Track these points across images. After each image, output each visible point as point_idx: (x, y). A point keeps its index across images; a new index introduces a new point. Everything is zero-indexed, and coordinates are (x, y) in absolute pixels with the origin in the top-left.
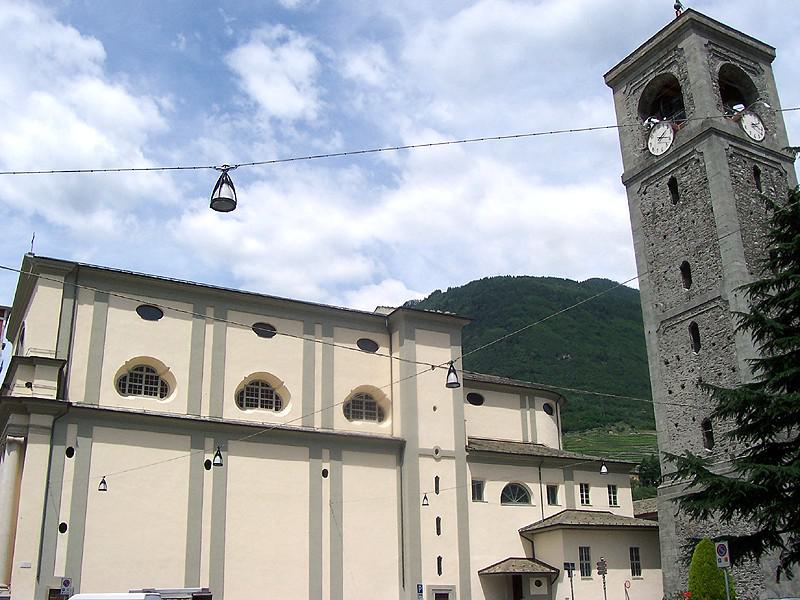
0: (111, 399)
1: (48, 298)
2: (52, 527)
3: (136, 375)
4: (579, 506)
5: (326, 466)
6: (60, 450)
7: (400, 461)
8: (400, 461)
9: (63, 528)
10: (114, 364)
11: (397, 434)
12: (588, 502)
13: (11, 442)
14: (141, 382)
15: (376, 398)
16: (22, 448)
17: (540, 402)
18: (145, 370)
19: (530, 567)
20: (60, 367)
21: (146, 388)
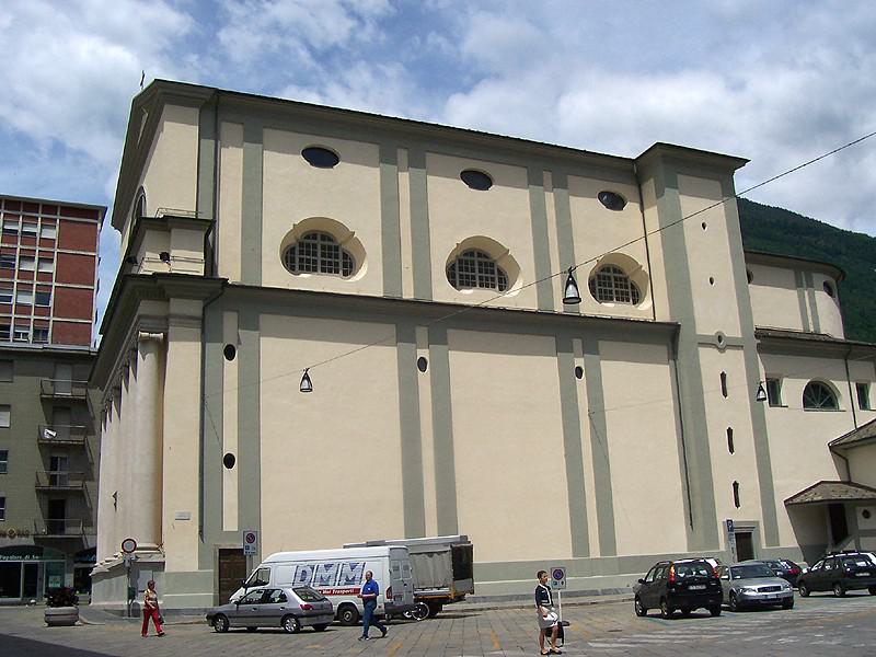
0: (275, 276)
1: (178, 139)
2: (213, 462)
3: (308, 246)
5: (579, 362)
6: (216, 349)
7: (673, 354)
8: (673, 354)
9: (229, 461)
10: (276, 232)
11: (663, 316)
13: (146, 341)
16: (162, 349)
17: (819, 279)
18: (476, 255)
20: (203, 227)
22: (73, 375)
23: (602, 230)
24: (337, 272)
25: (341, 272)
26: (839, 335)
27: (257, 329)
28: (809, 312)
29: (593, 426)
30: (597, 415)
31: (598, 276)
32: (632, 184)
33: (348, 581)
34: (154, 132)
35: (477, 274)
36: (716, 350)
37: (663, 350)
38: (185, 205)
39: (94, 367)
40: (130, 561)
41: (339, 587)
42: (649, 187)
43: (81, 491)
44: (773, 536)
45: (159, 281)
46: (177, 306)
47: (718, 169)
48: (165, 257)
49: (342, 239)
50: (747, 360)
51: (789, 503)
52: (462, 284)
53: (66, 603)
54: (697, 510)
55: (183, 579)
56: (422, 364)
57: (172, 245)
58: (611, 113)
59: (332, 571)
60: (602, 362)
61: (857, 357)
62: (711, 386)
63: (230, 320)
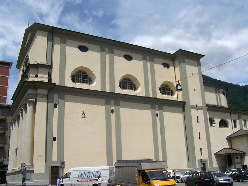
0: (69, 83)
1: (41, 41)
2: (50, 139)
3: (79, 75)
4: (244, 129)
5: (157, 112)
6: (51, 105)
7: (184, 110)
8: (184, 110)
9: (55, 139)
10: (70, 70)
11: (180, 99)
12: (246, 127)
13: (30, 101)
14: (81, 77)
15: (170, 87)
16: (35, 104)
17: (221, 90)
18: (82, 73)
19: (230, 152)
20: (48, 67)
21: (83, 80)
22: (2, 112)
23: (170, 75)
24: (87, 83)
25: (88, 83)
26: (226, 106)
27: (110, 105)
28: (150, 88)
29: (161, 131)
30: (162, 127)
31: (162, 88)
32: (172, 61)
33: (88, 177)
34: (33, 38)
35: (82, 79)
36: (195, 110)
37: (181, 109)
38: (43, 61)
39: (9, 111)
40: (24, 170)
41: (93, 179)
42: (177, 62)
43: (3, 147)
44: (211, 164)
45: (35, 83)
46: (40, 91)
47: (195, 58)
48: (37, 76)
49: (89, 73)
50: (204, 113)
51: (215, 154)
52: (123, 88)
53: (4, 183)
54: (190, 156)
55: (39, 175)
56: (112, 111)
57: (39, 72)
58: (168, 42)
59: (91, 174)
60: (121, 108)
61: (235, 113)
62: (194, 120)
63: (56, 96)
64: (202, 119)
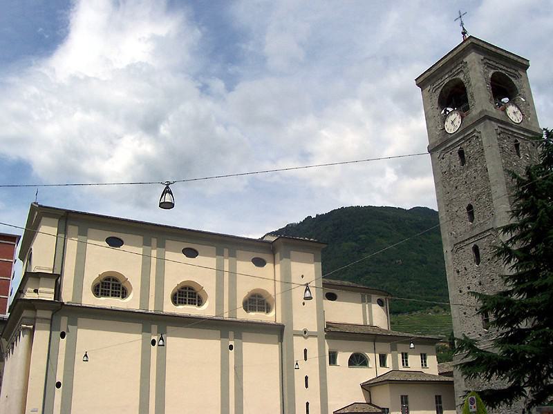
0: (89, 300)
2: (51, 385)
3: (183, 292)
4: (401, 368)
6: (57, 334)
8: (281, 340)
9: (58, 385)
10: (90, 278)
13: (24, 329)
15: (265, 297)
20: (56, 279)
36: (303, 338)
37: (276, 337)
46: (40, 314)
56: (231, 347)
62: (298, 356)
63: (64, 320)
64: (313, 353)
